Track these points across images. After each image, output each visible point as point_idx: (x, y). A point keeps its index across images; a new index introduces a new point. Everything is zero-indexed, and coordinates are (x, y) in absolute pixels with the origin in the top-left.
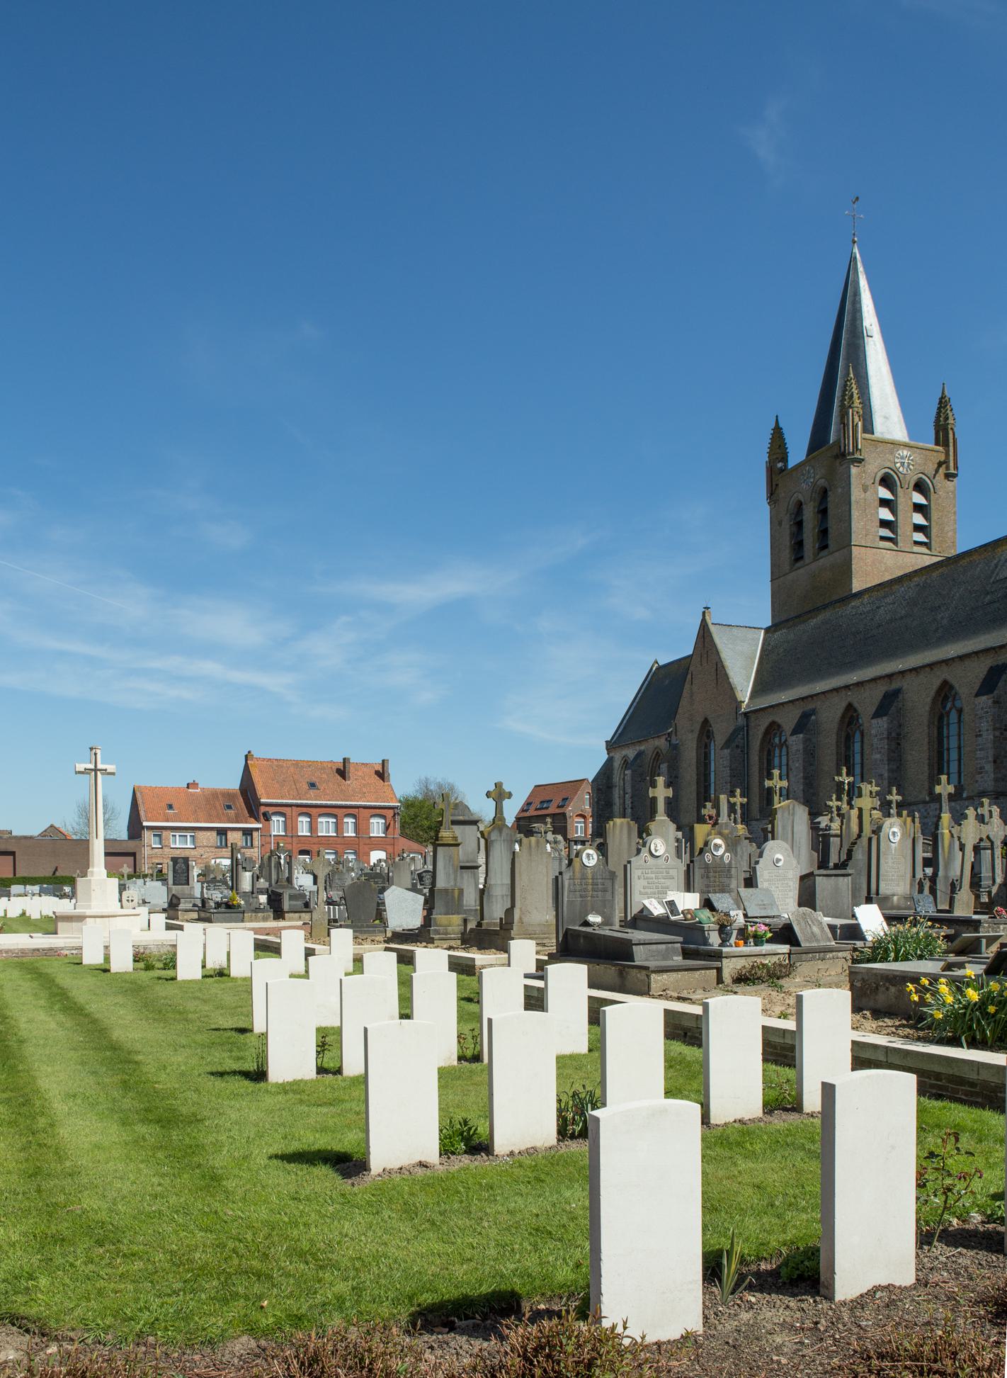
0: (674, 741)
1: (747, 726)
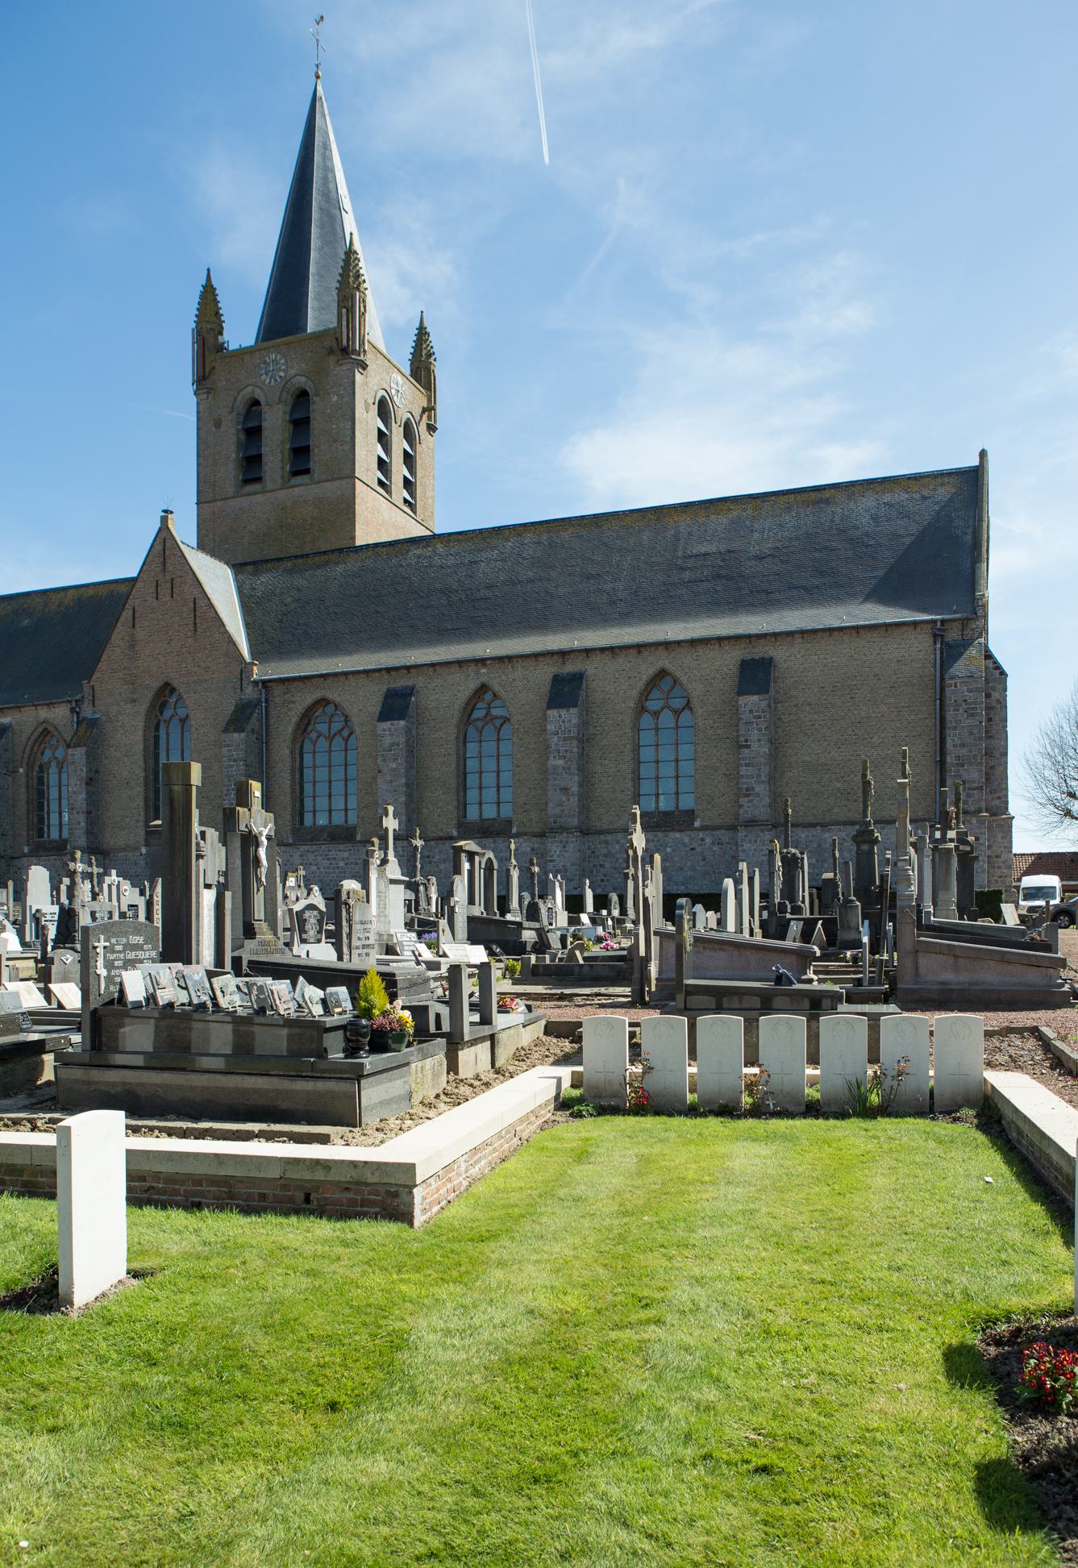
0: (87, 711)
1: (267, 701)
